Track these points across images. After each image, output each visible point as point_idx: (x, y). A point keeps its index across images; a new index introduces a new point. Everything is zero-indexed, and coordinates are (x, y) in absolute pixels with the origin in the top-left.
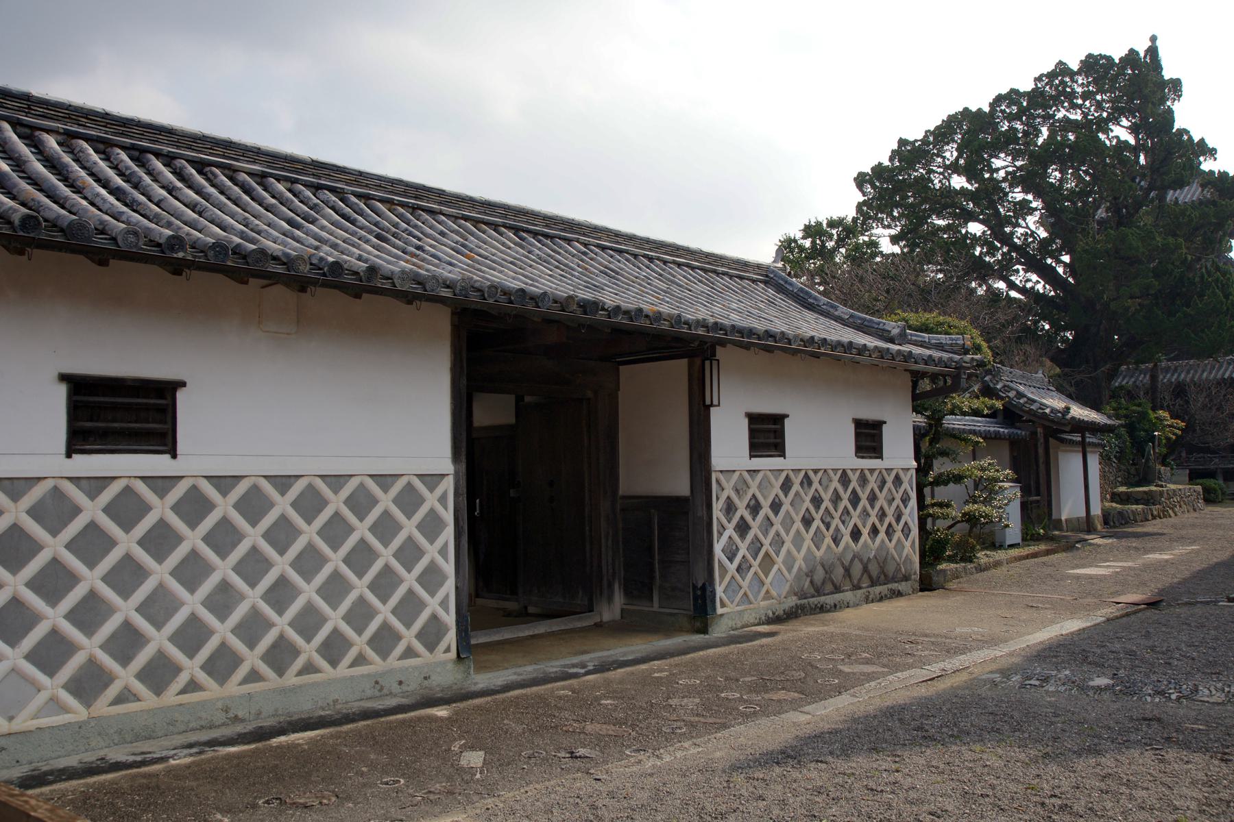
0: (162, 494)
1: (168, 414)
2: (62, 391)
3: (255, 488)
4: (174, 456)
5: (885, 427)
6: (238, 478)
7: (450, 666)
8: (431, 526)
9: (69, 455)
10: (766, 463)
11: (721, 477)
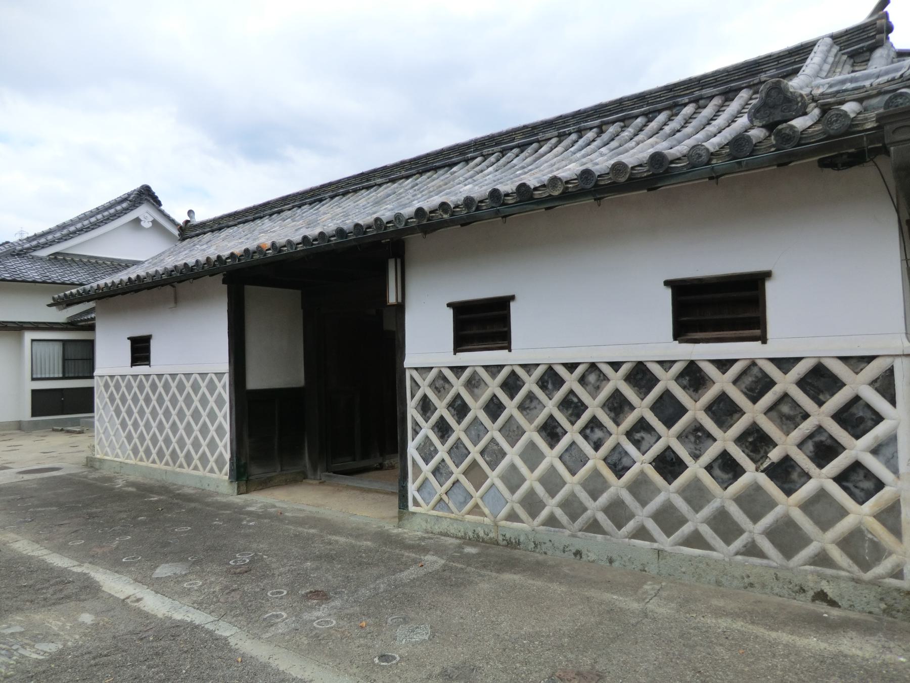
0: (494, 376)
1: (505, 320)
2: (129, 342)
3: (513, 373)
4: (510, 351)
5: (771, 288)
6: (502, 367)
7: (227, 484)
8: (219, 402)
9: (455, 354)
10: (141, 369)
11: (415, 374)
